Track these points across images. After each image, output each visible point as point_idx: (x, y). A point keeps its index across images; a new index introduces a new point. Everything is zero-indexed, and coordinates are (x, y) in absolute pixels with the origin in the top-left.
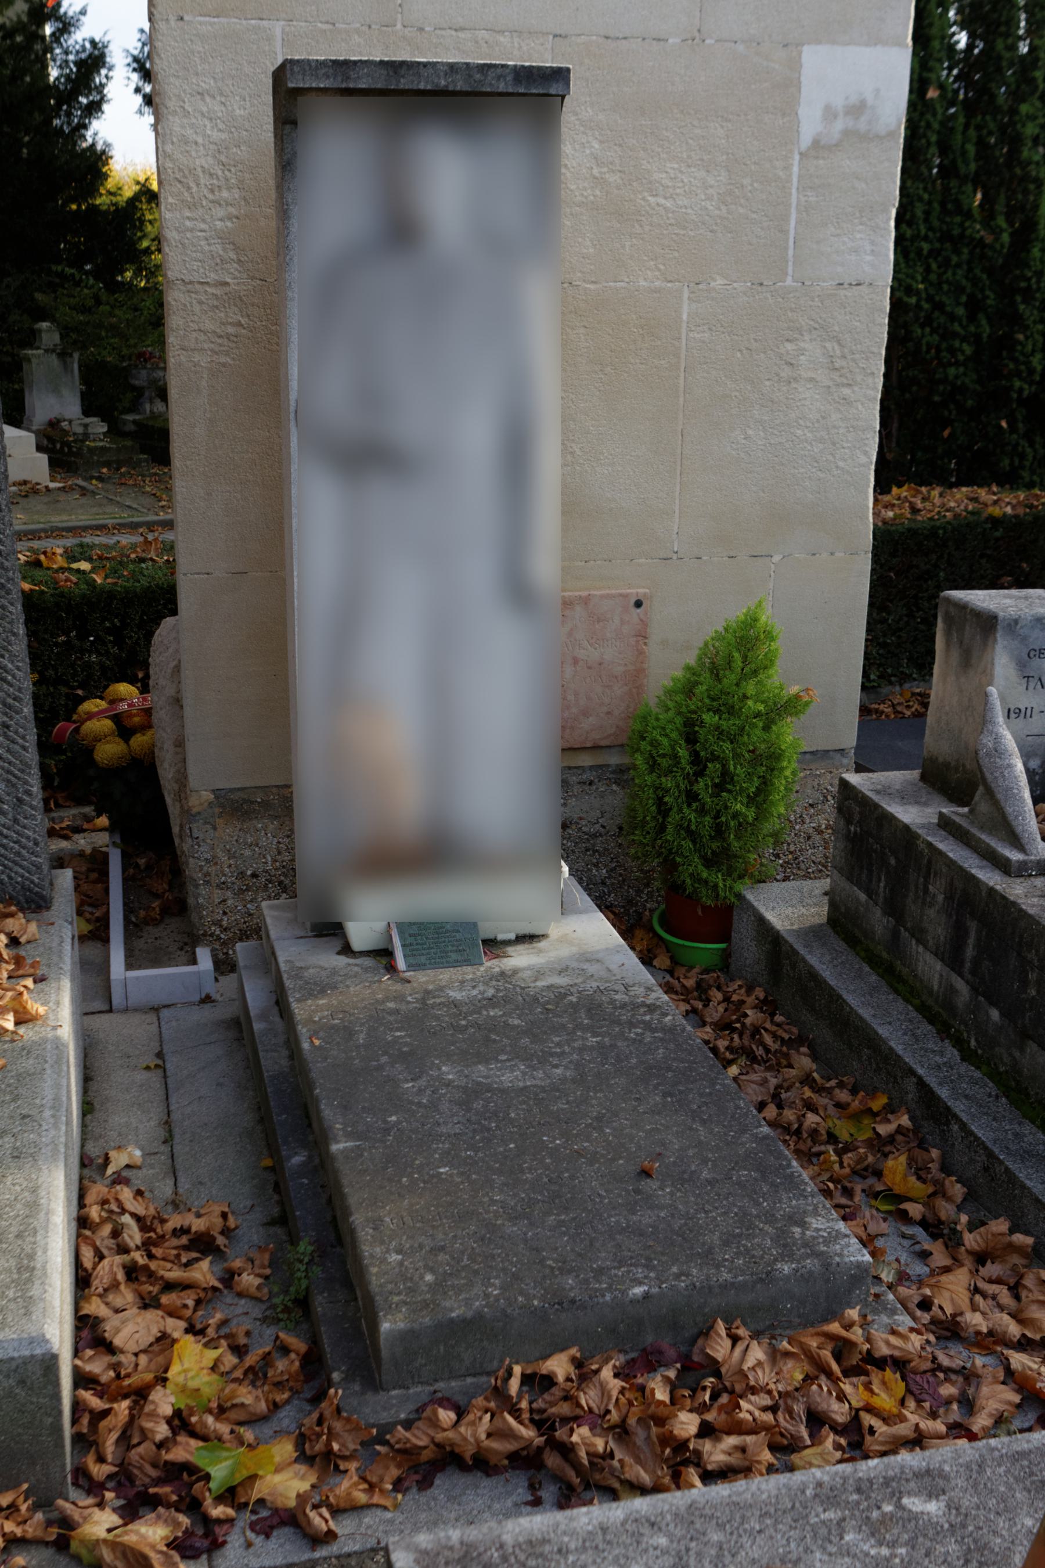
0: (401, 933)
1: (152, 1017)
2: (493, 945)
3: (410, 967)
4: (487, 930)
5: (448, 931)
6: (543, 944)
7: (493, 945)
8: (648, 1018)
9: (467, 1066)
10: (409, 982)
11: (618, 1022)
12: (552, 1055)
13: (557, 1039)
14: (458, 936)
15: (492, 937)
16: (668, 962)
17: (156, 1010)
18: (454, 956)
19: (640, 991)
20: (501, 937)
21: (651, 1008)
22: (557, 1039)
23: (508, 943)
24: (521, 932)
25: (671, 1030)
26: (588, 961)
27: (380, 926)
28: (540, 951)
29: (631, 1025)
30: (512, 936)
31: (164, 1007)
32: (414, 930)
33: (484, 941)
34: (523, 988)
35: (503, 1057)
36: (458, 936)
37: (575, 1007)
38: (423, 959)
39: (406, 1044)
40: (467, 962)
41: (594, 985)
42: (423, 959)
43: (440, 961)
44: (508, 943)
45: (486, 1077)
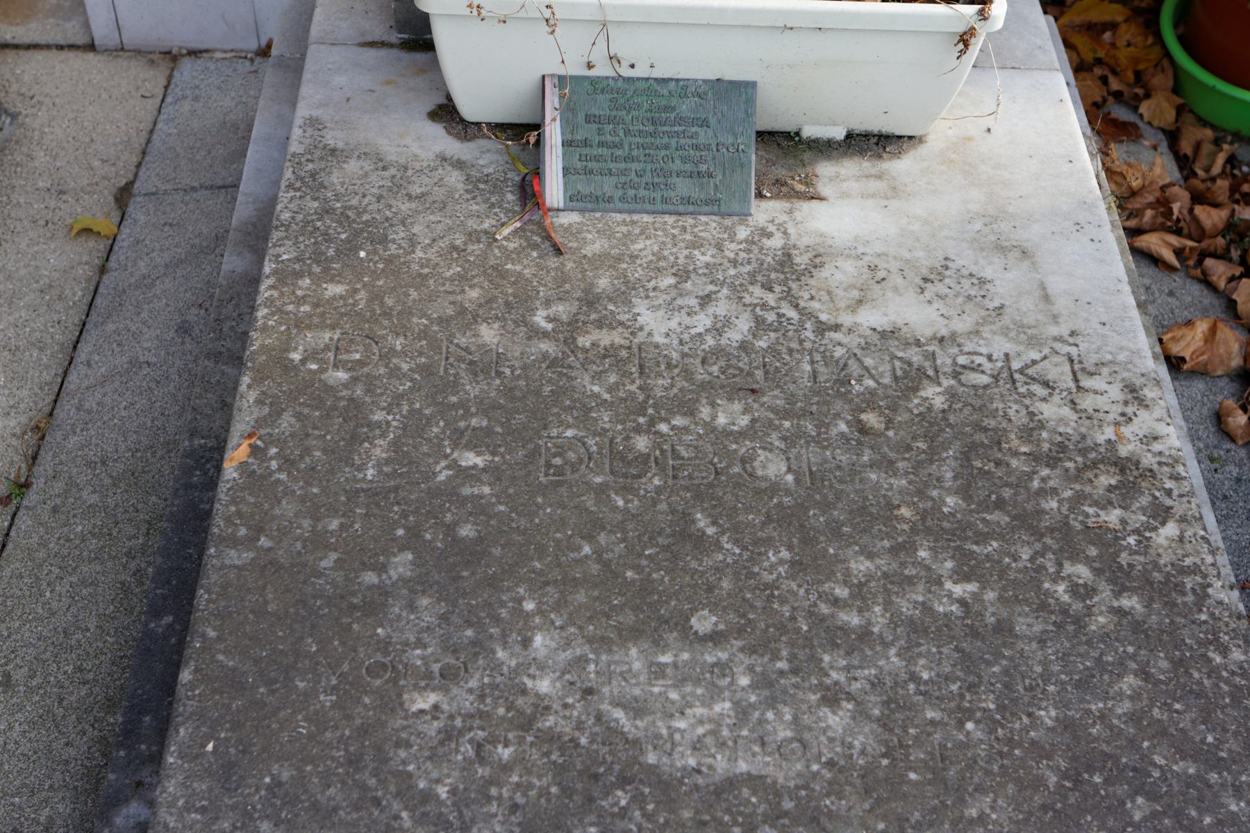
0: (568, 109)
1: (153, 79)
2: (788, 153)
3: (575, 200)
4: (777, 110)
5: (680, 120)
6: (902, 166)
7: (788, 153)
8: (1113, 517)
9: (601, 643)
10: (558, 251)
11: (1027, 521)
12: (835, 636)
13: (860, 566)
14: (704, 136)
15: (789, 127)
16: (1170, 115)
17: (172, 57)
18: (683, 187)
19: (1105, 394)
20: (809, 132)
21: (1131, 477)
22: (860, 566)
23: (824, 148)
24: (860, 126)
25: (1165, 586)
26: (1001, 248)
27: (525, 81)
28: (895, 191)
29: (1068, 541)
30: (839, 134)
31: (194, 53)
32: (601, 106)
33: (765, 137)
34: (822, 329)
35: (703, 622)
36: (704, 136)
37: (932, 426)
38: (607, 186)
39: (479, 509)
40: (713, 205)
41: (1001, 346)
42: (607, 186)
43: (648, 194)
44: (824, 148)
45: (637, 709)
